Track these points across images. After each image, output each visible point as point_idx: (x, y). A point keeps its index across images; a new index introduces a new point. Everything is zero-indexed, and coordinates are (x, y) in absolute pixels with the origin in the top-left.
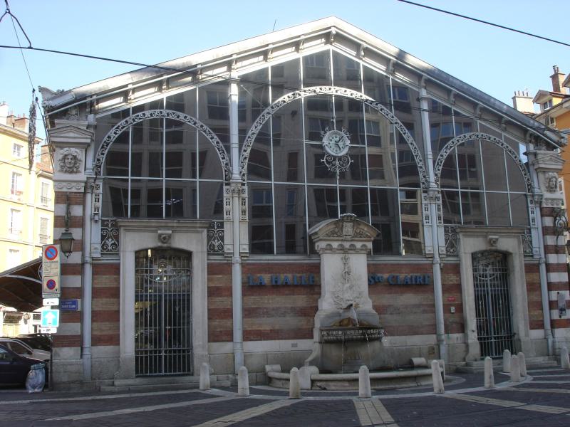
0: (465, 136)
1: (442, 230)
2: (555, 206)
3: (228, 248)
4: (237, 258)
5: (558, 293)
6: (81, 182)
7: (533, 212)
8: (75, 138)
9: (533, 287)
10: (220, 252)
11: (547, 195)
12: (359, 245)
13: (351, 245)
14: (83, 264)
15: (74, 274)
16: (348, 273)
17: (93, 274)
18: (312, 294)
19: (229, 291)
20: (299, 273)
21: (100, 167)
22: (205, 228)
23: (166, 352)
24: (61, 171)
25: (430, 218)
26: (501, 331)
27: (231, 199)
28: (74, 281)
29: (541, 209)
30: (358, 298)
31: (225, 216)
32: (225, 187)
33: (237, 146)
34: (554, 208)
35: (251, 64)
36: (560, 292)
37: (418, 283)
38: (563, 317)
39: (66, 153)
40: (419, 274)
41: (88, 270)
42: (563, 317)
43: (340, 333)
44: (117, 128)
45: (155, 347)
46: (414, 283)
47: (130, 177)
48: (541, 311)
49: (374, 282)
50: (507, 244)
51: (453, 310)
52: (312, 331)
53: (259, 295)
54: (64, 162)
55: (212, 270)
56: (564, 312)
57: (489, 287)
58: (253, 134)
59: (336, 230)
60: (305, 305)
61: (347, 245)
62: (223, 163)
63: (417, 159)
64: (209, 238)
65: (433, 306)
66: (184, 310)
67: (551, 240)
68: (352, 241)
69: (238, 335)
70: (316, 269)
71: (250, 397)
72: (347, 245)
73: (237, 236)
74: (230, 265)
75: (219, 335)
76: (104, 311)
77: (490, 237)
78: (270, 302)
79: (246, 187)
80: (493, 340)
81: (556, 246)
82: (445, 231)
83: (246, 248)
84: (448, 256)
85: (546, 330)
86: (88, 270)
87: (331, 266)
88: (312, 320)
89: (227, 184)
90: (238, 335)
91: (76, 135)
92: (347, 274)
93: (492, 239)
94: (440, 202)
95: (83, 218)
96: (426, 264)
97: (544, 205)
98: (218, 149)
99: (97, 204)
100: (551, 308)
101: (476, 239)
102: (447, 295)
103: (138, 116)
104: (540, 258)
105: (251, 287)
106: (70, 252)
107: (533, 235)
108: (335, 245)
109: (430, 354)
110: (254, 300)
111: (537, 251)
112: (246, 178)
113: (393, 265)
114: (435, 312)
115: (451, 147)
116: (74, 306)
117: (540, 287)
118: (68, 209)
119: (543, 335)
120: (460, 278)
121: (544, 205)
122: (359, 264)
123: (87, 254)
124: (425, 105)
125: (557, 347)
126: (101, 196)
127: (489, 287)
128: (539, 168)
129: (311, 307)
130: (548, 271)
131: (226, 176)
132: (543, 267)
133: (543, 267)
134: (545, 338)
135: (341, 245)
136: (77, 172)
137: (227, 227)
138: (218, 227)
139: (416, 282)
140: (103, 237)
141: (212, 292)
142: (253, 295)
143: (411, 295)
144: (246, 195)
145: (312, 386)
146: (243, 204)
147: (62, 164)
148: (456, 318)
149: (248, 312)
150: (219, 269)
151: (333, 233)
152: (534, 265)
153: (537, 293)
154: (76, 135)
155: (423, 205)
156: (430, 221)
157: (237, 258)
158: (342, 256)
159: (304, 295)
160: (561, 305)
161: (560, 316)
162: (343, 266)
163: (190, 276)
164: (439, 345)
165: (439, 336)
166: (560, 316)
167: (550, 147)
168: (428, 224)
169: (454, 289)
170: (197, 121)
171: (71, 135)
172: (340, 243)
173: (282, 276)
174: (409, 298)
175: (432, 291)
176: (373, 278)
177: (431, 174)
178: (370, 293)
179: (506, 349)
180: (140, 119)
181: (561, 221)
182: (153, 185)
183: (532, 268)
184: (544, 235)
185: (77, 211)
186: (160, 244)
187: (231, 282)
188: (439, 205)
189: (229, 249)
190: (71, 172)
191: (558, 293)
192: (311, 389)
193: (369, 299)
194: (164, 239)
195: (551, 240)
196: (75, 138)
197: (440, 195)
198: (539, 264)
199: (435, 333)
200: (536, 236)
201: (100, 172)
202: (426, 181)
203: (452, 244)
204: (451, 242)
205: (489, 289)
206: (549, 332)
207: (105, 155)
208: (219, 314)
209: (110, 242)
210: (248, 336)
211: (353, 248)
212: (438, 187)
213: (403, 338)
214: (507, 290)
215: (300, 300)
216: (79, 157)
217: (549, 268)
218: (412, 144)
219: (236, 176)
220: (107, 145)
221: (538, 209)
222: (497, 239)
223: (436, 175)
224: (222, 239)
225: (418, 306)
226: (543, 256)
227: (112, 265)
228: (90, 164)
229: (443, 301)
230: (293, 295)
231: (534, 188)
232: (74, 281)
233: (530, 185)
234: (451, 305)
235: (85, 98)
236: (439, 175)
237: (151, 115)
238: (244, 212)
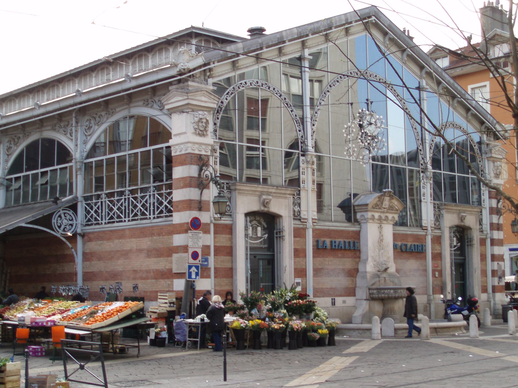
0: (246, 83)
2: (203, 153)
3: (303, 215)
5: (498, 263)
6: (209, 145)
7: (424, 188)
8: (206, 102)
9: (483, 257)
12: (390, 216)
16: (382, 240)
18: (355, 258)
20: (347, 239)
24: (195, 134)
25: (426, 195)
27: (306, 169)
31: (302, 185)
32: (301, 158)
34: (201, 155)
37: (334, 247)
39: (201, 116)
44: (227, 94)
47: (456, 174)
48: (485, 278)
50: (470, 221)
51: (437, 273)
52: (355, 290)
53: (323, 257)
54: (198, 126)
59: (378, 203)
60: (350, 267)
61: (383, 216)
67: (495, 219)
72: (383, 216)
76: (222, 268)
77: (462, 214)
78: (330, 263)
81: (498, 224)
85: (489, 294)
88: (354, 280)
89: (303, 155)
91: (180, 98)
94: (315, 167)
96: (421, 235)
98: (296, 121)
104: (487, 234)
108: (377, 215)
109: (424, 311)
111: (485, 228)
113: (403, 235)
114: (426, 276)
115: (232, 93)
116: (206, 263)
117: (486, 258)
118: (201, 170)
119: (426, 300)
120: (441, 248)
122: (388, 231)
128: (491, 157)
129: (354, 269)
130: (492, 244)
131: (302, 147)
132: (488, 242)
133: (488, 242)
134: (488, 301)
137: (303, 193)
139: (418, 250)
142: (319, 257)
145: (395, 333)
146: (431, 185)
147: (196, 127)
148: (438, 282)
149: (317, 271)
151: (376, 205)
154: (180, 98)
157: (310, 224)
159: (350, 258)
163: (306, 240)
164: (430, 304)
166: (499, 283)
167: (496, 138)
169: (437, 256)
171: (203, 99)
172: (379, 214)
175: (425, 258)
178: (395, 258)
181: (207, 173)
183: (483, 242)
186: (262, 208)
187: (305, 245)
189: (305, 215)
191: (498, 263)
192: (395, 337)
193: (394, 264)
194: (265, 204)
195: (495, 219)
196: (206, 102)
197: (315, 159)
198: (486, 238)
199: (426, 294)
200: (486, 213)
202: (424, 162)
203: (438, 218)
206: (491, 295)
212: (216, 139)
215: (347, 263)
217: (493, 242)
222: (466, 216)
223: (215, 124)
226: (489, 231)
227: (226, 226)
230: (344, 258)
231: (486, 173)
233: (304, 142)
236: (218, 125)
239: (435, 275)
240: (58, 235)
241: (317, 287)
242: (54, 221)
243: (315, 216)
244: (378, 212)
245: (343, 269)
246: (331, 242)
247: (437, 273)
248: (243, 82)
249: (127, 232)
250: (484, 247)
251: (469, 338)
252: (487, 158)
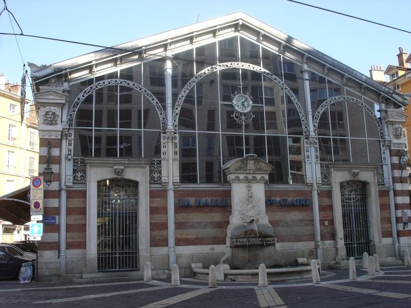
0: (335, 98)
1: (319, 166)
3: (164, 179)
4: (171, 186)
5: (403, 211)
6: (58, 131)
7: (384, 153)
8: (54, 99)
9: (384, 207)
10: (159, 182)
11: (395, 141)
12: (259, 177)
13: (253, 177)
14: (60, 191)
15: (54, 197)
16: (251, 197)
17: (67, 198)
18: (225, 212)
19: (165, 210)
20: (215, 197)
21: (72, 120)
22: (148, 164)
23: (119, 254)
25: (310, 157)
26: (361, 239)
27: (167, 143)
28: (54, 203)
29: (390, 151)
30: (258, 215)
31: (162, 156)
32: (162, 135)
33: (171, 105)
34: (399, 150)
35: (181, 46)
36: (404, 211)
37: (301, 204)
38: (406, 229)
40: (302, 198)
41: (64, 195)
42: (406, 229)
44: (85, 92)
45: (112, 250)
46: (298, 204)
47: (94, 128)
48: (390, 224)
49: (269, 203)
50: (366, 176)
51: (326, 223)
52: (225, 239)
53: (187, 212)
54: (46, 117)
55: (153, 195)
56: (406, 225)
57: (353, 207)
58: (182, 96)
59: (243, 166)
60: (220, 220)
61: (250, 177)
62: (161, 117)
63: (301, 115)
64: (151, 172)
65: (312, 220)
66: (133, 223)
67: (397, 173)
68: (254, 174)
69: (171, 241)
70: (228, 194)
71: (180, 286)
72: (250, 177)
73: (171, 170)
74: (166, 191)
75: (158, 241)
76: (75, 224)
77: (354, 171)
78: (195, 217)
79: (177, 135)
80: (356, 245)
81: (401, 177)
82: (321, 167)
83: (177, 179)
84: (323, 184)
85: (394, 238)
86: (64, 195)
87: (238, 192)
88: (225, 231)
89: (163, 133)
90: (171, 241)
91: (55, 98)
92: (250, 198)
93: (355, 172)
94: (318, 146)
95: (60, 157)
96: (307, 191)
97: (392, 148)
98: (157, 107)
99: (70, 147)
100: (397, 222)
101: (343, 172)
102: (322, 213)
103: (99, 84)
104: (390, 186)
105: (181, 207)
106: (51, 182)
107: (384, 169)
108: (242, 177)
109: (310, 255)
110: (183, 216)
112: (177, 128)
113: (283, 191)
115: (325, 106)
116: (53, 221)
117: (390, 207)
119: (392, 241)
120: (332, 201)
121: (392, 148)
122: (259, 190)
123: (63, 184)
124: (306, 76)
125: (402, 250)
126: (73, 141)
127: (353, 207)
128: (389, 121)
129: (224, 222)
130: (395, 195)
131: (163, 127)
132: (392, 193)
133: (392, 193)
134: (393, 244)
135: (246, 177)
136: (56, 124)
137: (164, 164)
138: (157, 164)
139: (300, 203)
140: (74, 171)
141: (153, 211)
142: (182, 213)
143: (296, 213)
144: (177, 141)
145: (225, 278)
146: (176, 147)
147: (45, 118)
148: (329, 230)
149: (179, 225)
150: (158, 194)
151: (240, 168)
152: (385, 191)
153: (387, 211)
154: (55, 98)
155: (305, 148)
156: (310, 159)
157: (171, 186)
158: (246, 184)
159: (219, 212)
160: (404, 220)
161: (404, 228)
162: (247, 192)
163: (137, 199)
164: (316, 249)
165: (316, 242)
166: (404, 228)
167: (397, 106)
168: (308, 162)
169: (327, 208)
170: (142, 88)
172: (245, 175)
173: (204, 199)
174: (295, 215)
175: (312, 210)
176: (269, 201)
177: (311, 126)
178: (267, 211)
179: (365, 251)
180: (101, 86)
181: (404, 160)
182: (110, 134)
183: (383, 194)
184: (392, 169)
185: (55, 152)
186: (115, 176)
187: (167, 204)
188: (316, 148)
189: (165, 180)
190: (52, 124)
191: (403, 211)
192: (224, 281)
193: (266, 216)
194: (118, 172)
195: (397, 173)
196: (54, 99)
197: (317, 141)
198: (389, 190)
199: (314, 240)
200: (387, 170)
201: (72, 124)
203: (326, 176)
205: (353, 208)
206: (396, 240)
207: (76, 112)
208: (158, 227)
209: (79, 175)
210: (179, 242)
211: (254, 179)
212: (316, 135)
213: (291, 244)
214: (366, 209)
215: (217, 217)
216: (57, 113)
218: (297, 104)
219: (170, 127)
220: (77, 105)
221: (388, 151)
222: (358, 173)
223: (314, 126)
224: (160, 172)
225: (302, 221)
226: (391, 185)
227: (80, 191)
228: (65, 118)
229: (320, 217)
231: (385, 136)
232: (54, 203)
233: (382, 133)
234: (326, 220)
235: (61, 71)
236: (317, 126)
237: (109, 83)
238: (176, 153)
243: (176, 180)
248: (333, 98)
252: (386, 122)
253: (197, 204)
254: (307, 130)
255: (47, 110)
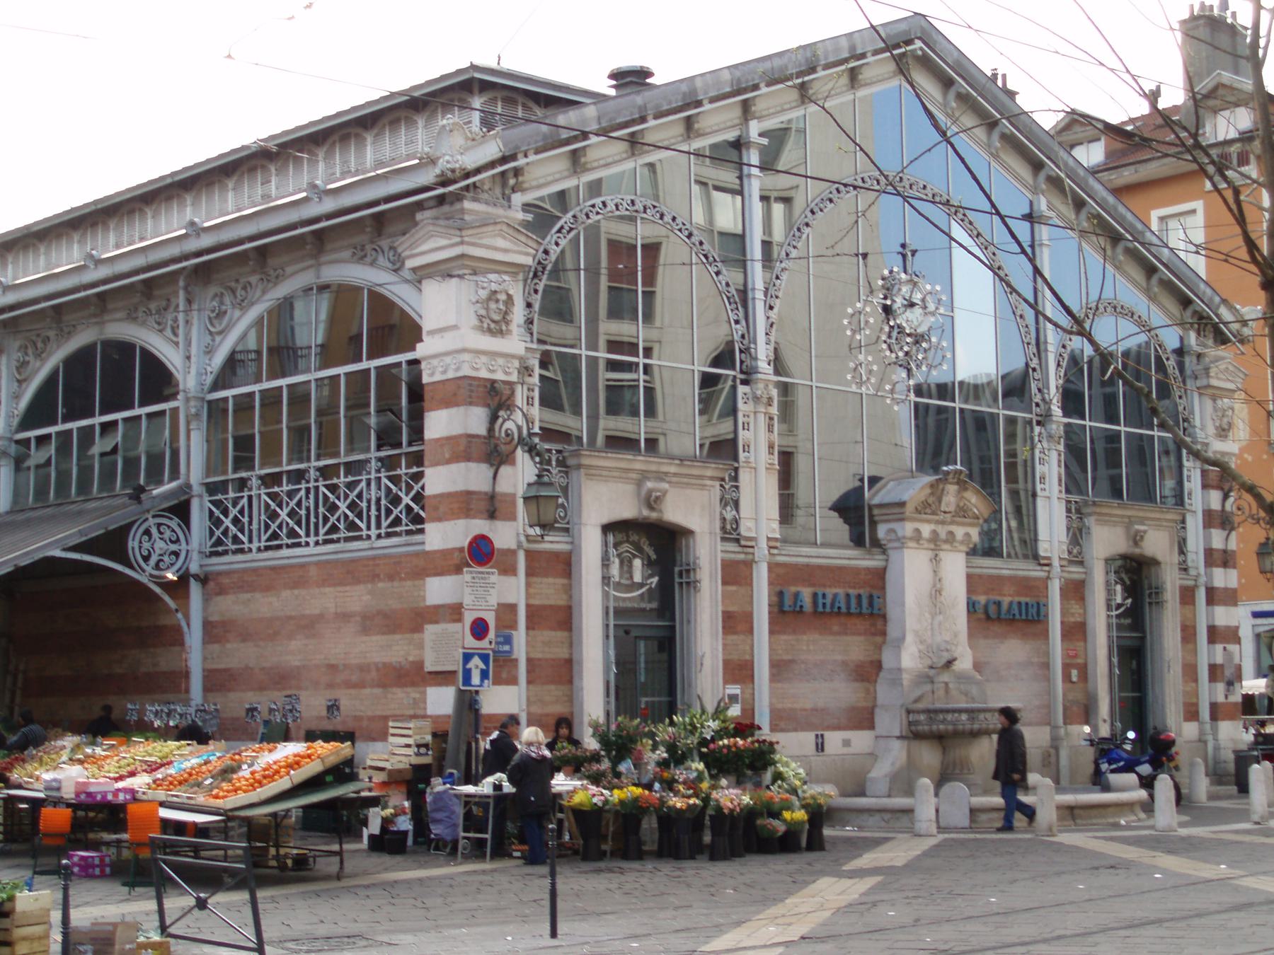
0: (604, 204)
3: (746, 528)
5: (1225, 648)
6: (513, 356)
8: (506, 251)
9: (1188, 634)
12: (960, 532)
16: (939, 592)
18: (874, 634)
20: (854, 588)
25: (1047, 479)
27: (752, 416)
31: (742, 456)
32: (741, 389)
34: (493, 382)
37: (820, 609)
43: (922, 717)
44: (559, 231)
47: (1122, 428)
48: (1194, 685)
50: (1157, 543)
51: (1074, 673)
53: (794, 632)
54: (487, 309)
59: (930, 500)
60: (861, 658)
61: (942, 531)
67: (1218, 539)
72: (942, 531)
76: (547, 660)
77: (1137, 527)
78: (811, 647)
81: (1225, 551)
85: (1202, 723)
88: (872, 689)
89: (745, 382)
91: (444, 242)
94: (774, 410)
96: (1036, 579)
98: (728, 298)
104: (1198, 575)
108: (926, 530)
109: (1044, 766)
113: (992, 578)
115: (571, 229)
116: (507, 648)
117: (1195, 634)
119: (1048, 737)
120: (1085, 610)
122: (955, 567)
128: (1209, 386)
129: (872, 662)
130: (1211, 601)
131: (742, 362)
132: (1201, 595)
133: (1201, 595)
134: (1200, 740)
139: (1027, 614)
142: (785, 633)
145: (972, 820)
147: (483, 312)
148: (1077, 695)
149: (779, 668)
151: (926, 504)
154: (444, 242)
157: (762, 550)
159: (860, 634)
162: (932, 573)
163: (752, 591)
164: (1057, 749)
165: (1055, 728)
166: (1226, 697)
167: (1221, 339)
169: (1076, 631)
172: (933, 527)
173: (830, 592)
175: (1045, 634)
178: (971, 635)
181: (509, 425)
183: (1187, 596)
186: (646, 512)
187: (751, 603)
189: (749, 529)
191: (1225, 648)
192: (971, 829)
193: (968, 649)
194: (652, 501)
195: (1218, 539)
196: (506, 251)
197: (774, 393)
198: (1196, 586)
199: (1049, 724)
200: (1194, 524)
203: (1077, 535)
204: (1074, 534)
206: (1208, 727)
212: (532, 342)
215: (854, 647)
222: (1145, 532)
223: (529, 305)
226: (1202, 570)
227: (556, 555)
230: (846, 634)
231: (1194, 427)
233: (748, 349)
236: (537, 307)
239: (1070, 676)
240: (144, 579)
241: (779, 706)
242: (132, 544)
244: (929, 521)
245: (844, 663)
246: (815, 595)
247: (1074, 673)
249: (313, 571)
250: (1192, 607)
251: (1153, 832)
253: (798, 609)
254: (1043, 400)
255: (494, 287)
